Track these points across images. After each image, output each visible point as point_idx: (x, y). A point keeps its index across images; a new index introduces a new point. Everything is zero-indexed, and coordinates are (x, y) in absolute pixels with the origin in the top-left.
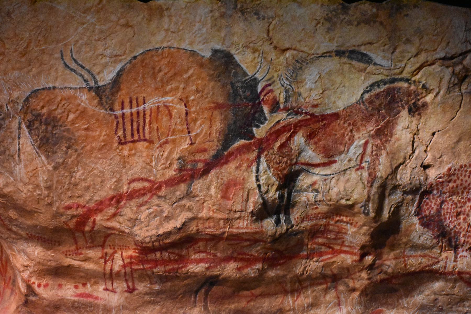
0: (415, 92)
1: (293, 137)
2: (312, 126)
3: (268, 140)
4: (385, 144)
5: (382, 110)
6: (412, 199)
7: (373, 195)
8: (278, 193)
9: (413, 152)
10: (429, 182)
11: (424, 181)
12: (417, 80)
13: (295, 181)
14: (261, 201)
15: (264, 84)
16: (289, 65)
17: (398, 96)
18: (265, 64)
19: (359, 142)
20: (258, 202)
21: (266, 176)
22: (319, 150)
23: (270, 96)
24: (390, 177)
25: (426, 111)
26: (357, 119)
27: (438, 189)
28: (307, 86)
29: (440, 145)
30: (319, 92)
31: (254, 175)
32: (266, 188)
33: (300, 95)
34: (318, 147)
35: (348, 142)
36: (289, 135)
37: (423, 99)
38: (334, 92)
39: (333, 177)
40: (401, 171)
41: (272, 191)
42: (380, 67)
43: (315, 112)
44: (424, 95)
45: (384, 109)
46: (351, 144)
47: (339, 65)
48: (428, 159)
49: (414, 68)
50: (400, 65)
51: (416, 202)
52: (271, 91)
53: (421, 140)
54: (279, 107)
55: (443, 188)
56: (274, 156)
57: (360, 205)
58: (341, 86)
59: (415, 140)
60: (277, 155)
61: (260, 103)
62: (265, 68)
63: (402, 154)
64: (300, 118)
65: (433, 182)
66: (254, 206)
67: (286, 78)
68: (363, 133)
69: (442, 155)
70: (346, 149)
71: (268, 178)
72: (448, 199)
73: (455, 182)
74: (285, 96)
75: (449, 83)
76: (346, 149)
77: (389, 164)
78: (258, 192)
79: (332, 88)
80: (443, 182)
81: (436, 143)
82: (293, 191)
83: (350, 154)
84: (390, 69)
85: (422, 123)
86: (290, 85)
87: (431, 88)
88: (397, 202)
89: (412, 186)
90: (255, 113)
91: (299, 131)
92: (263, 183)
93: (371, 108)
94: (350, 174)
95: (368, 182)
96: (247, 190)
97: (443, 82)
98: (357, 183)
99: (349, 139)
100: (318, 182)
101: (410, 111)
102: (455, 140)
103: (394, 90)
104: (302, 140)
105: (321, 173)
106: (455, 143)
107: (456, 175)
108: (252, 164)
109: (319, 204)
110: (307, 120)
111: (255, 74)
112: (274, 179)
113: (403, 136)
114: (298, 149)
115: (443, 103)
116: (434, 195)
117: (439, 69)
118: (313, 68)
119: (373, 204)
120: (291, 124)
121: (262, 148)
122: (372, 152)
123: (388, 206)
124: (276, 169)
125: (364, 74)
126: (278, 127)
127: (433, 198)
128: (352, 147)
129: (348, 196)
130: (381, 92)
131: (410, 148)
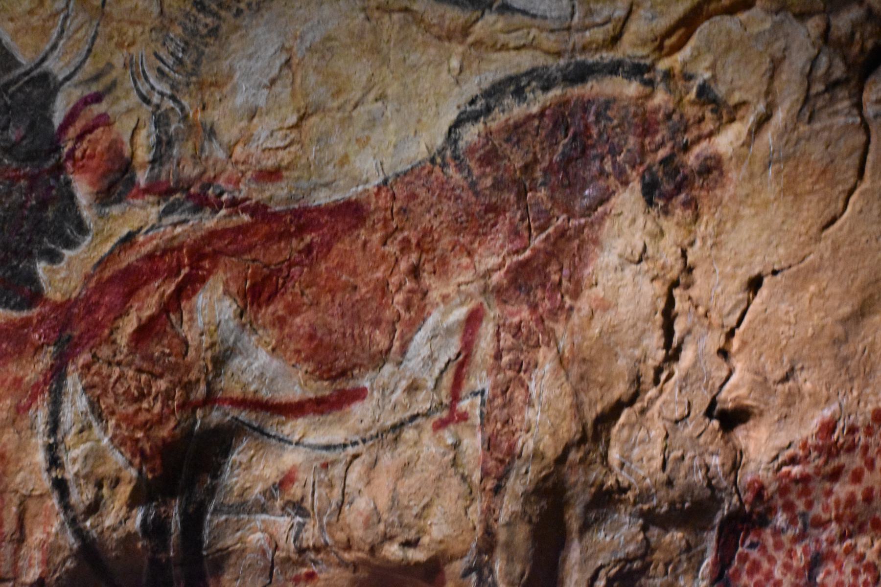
0: (668, 117)
1: (189, 298)
2: (259, 253)
3: (91, 308)
4: (549, 323)
5: (534, 189)
6: (689, 548)
7: (508, 524)
8: (138, 515)
9: (673, 355)
10: (749, 478)
11: (726, 476)
12: (678, 68)
13: (216, 471)
14: (70, 541)
15: (77, 94)
16: (172, 21)
17: (600, 134)
18: (81, 17)
19: (445, 314)
20: (60, 548)
21: (88, 445)
22: (292, 347)
23: (97, 141)
24: (574, 456)
25: (718, 192)
26: (436, 224)
27: (789, 507)
28: (239, 100)
29: (783, 328)
30: (284, 119)
31: (40, 440)
32: (89, 494)
33: (212, 133)
34: (290, 336)
35: (405, 316)
36: (170, 288)
37: (704, 144)
38: (342, 121)
39: (356, 456)
40: (625, 433)
41: (117, 505)
42: (527, 20)
43: (271, 198)
44: (708, 126)
45: (544, 184)
46: (415, 325)
47: (362, 16)
48: (736, 387)
49: (663, 23)
50: (606, 13)
51: (708, 560)
52: (103, 121)
53: (701, 310)
54: (132, 182)
55: (810, 505)
56: (117, 371)
57: (459, 566)
58: (371, 96)
59: (678, 306)
60: (129, 365)
61: (59, 168)
62: (79, 35)
63: (622, 364)
64: (210, 222)
65: (766, 476)
66: (46, 562)
67: (160, 71)
68: (461, 279)
69: (792, 369)
70: (397, 344)
71: (96, 456)
72: (837, 548)
73: (857, 477)
74: (153, 139)
75: (809, 77)
76: (397, 344)
77: (568, 401)
78: (57, 507)
79: (335, 104)
80: (805, 479)
81: (766, 321)
82: (211, 508)
83: (414, 363)
84: (569, 29)
85: (704, 239)
86: (173, 98)
87: (736, 98)
88: (621, 555)
89: (675, 493)
90: (43, 204)
91: (210, 272)
92: (76, 475)
93: (489, 182)
94: (416, 443)
95: (485, 474)
96: (16, 500)
97: (784, 77)
98: (438, 479)
99: (408, 306)
100: (301, 476)
101: (650, 192)
102: (846, 310)
103: (585, 110)
104: (227, 309)
105: (311, 439)
106: (844, 321)
107: (858, 450)
108: (33, 398)
109: (315, 563)
110: (241, 230)
111: (43, 60)
112: (117, 459)
113: (626, 292)
114: (213, 345)
115: (787, 158)
116: (778, 532)
117: (767, 25)
118: (260, 31)
119: (510, 560)
120: (180, 248)
121: (70, 338)
122: (498, 356)
123: (582, 570)
124: (128, 419)
125: (460, 49)
126: (130, 258)
127: (778, 546)
128: (420, 337)
129: (409, 527)
130: (530, 117)
131: (654, 341)
